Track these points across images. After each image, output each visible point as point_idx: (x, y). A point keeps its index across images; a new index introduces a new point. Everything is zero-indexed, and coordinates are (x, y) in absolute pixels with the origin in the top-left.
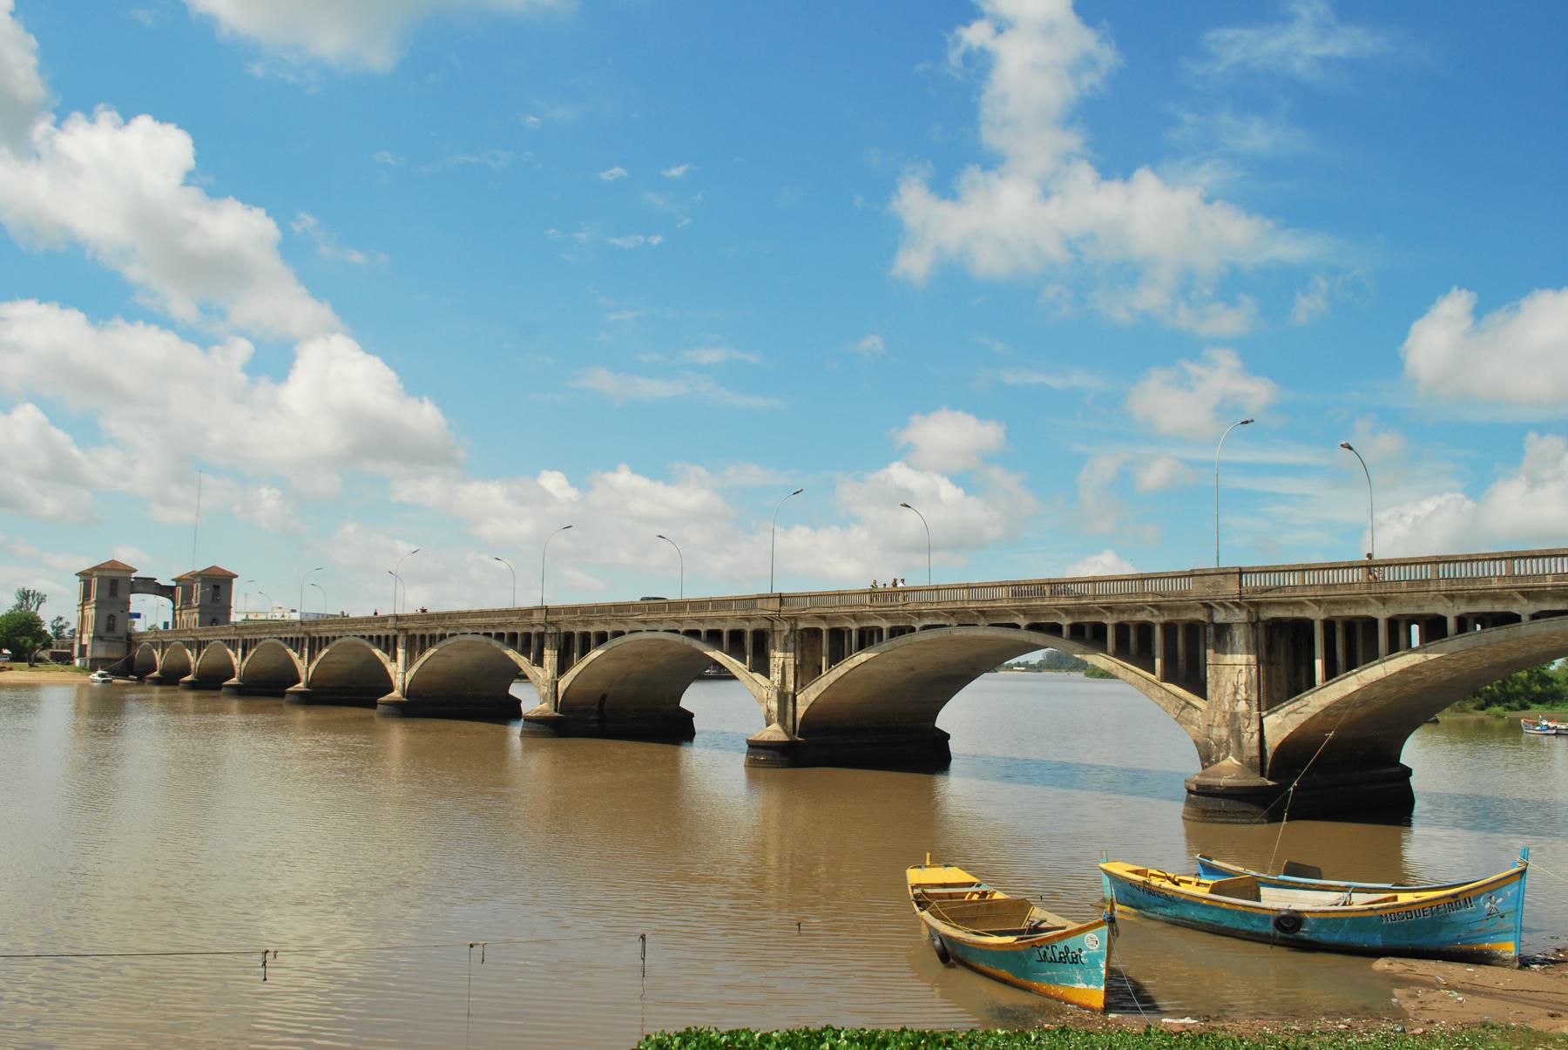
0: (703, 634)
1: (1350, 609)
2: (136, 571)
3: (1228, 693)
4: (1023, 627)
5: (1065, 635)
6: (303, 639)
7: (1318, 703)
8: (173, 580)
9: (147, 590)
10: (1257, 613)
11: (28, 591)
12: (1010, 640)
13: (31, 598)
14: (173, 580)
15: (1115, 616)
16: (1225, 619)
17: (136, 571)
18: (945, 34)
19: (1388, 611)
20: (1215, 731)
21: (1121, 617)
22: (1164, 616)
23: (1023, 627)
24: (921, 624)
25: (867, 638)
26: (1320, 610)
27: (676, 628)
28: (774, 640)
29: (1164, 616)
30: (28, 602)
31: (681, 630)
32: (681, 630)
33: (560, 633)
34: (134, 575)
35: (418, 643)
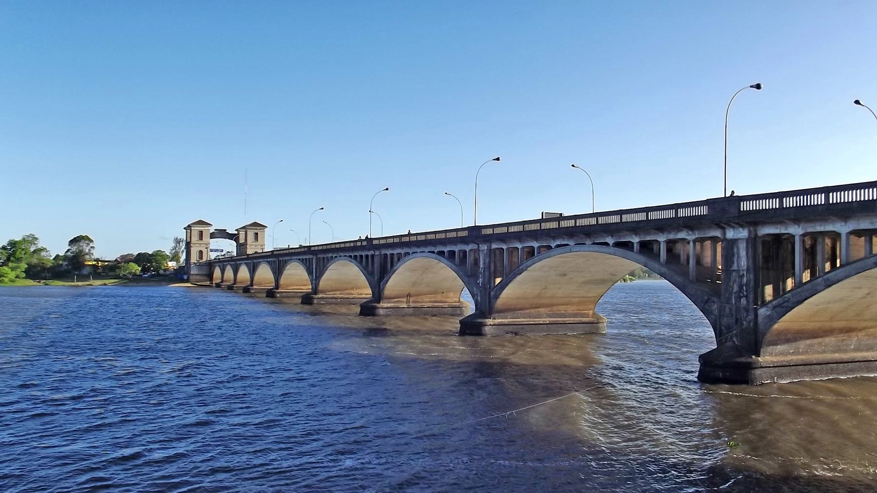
0: (635, 245)
1: (821, 226)
3: (734, 291)
4: (611, 245)
5: (635, 250)
6: (276, 261)
7: (796, 300)
8: (236, 230)
9: (222, 237)
10: (756, 231)
11: (181, 239)
12: (63, 281)
13: (181, 243)
14: (236, 230)
15: (665, 236)
16: (733, 236)
18: (753, 416)
19: (849, 227)
20: (725, 320)
21: (669, 236)
22: (695, 235)
23: (611, 245)
24: (555, 244)
25: (350, 256)
26: (799, 227)
27: (433, 250)
28: (738, 249)
29: (695, 235)
30: (179, 245)
31: (348, 255)
32: (348, 255)
33: (381, 255)
35: (322, 261)
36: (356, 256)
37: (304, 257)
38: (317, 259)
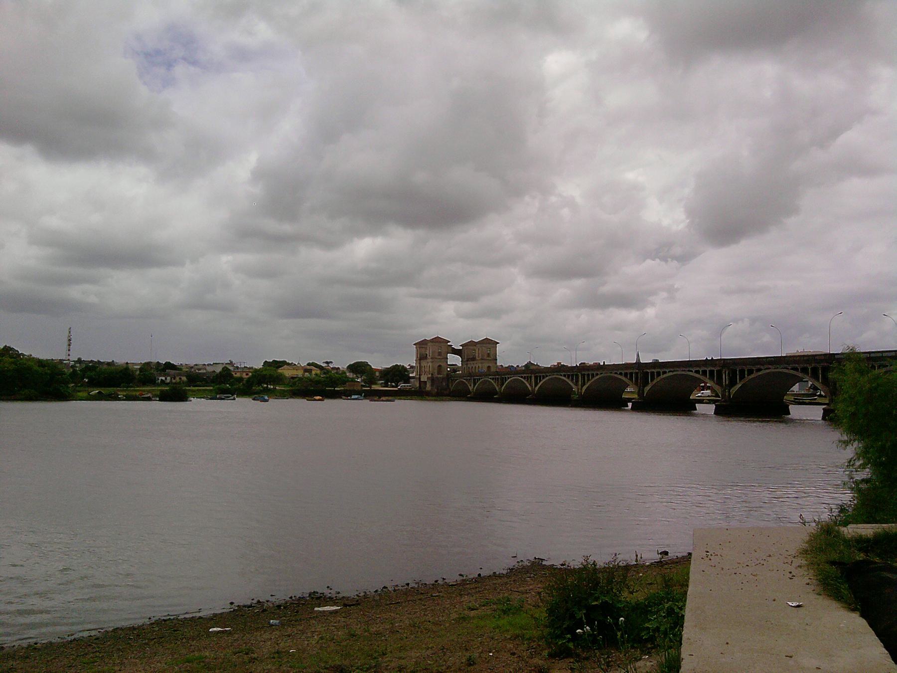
2: (449, 342)
6: (531, 377)
17: (449, 342)
34: (449, 344)
36: (467, 379)
37: (629, 371)
38: (535, 377)
